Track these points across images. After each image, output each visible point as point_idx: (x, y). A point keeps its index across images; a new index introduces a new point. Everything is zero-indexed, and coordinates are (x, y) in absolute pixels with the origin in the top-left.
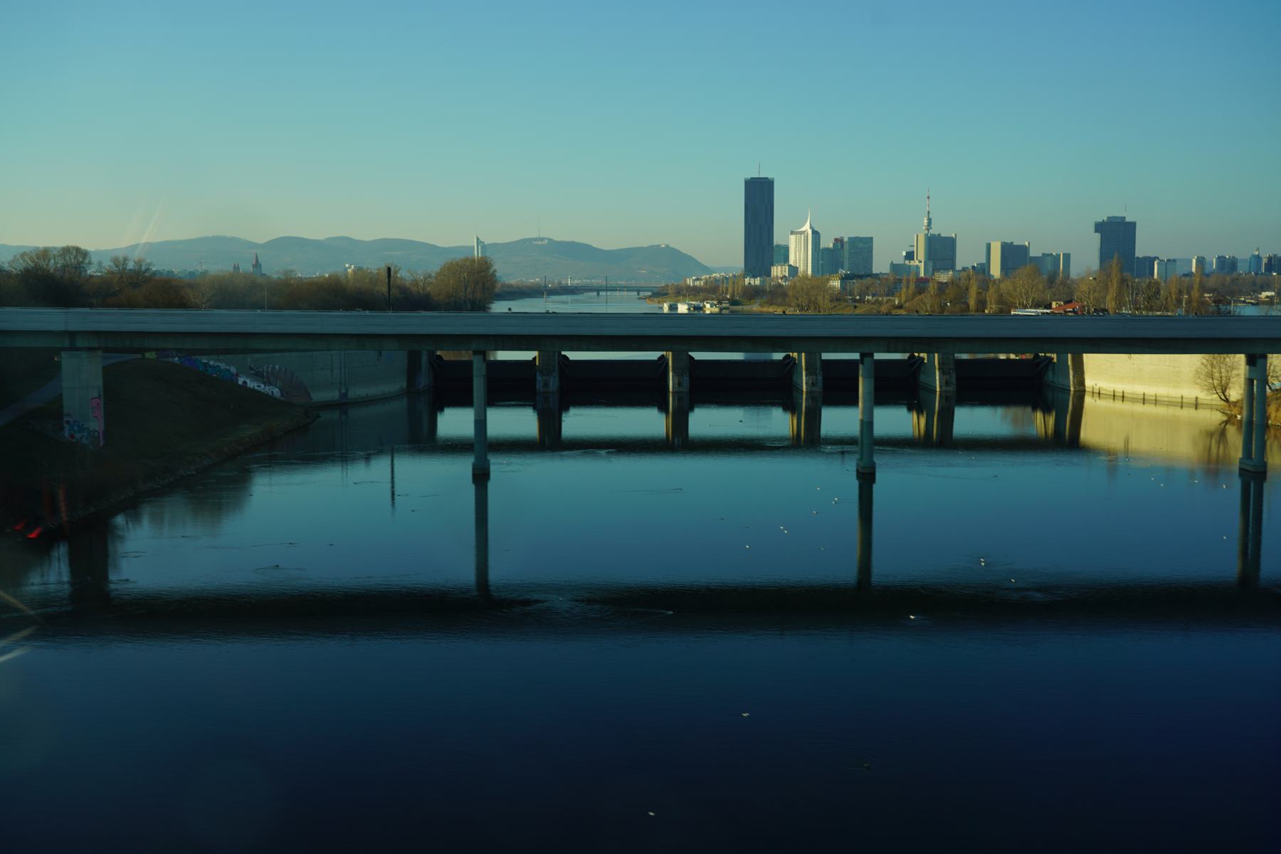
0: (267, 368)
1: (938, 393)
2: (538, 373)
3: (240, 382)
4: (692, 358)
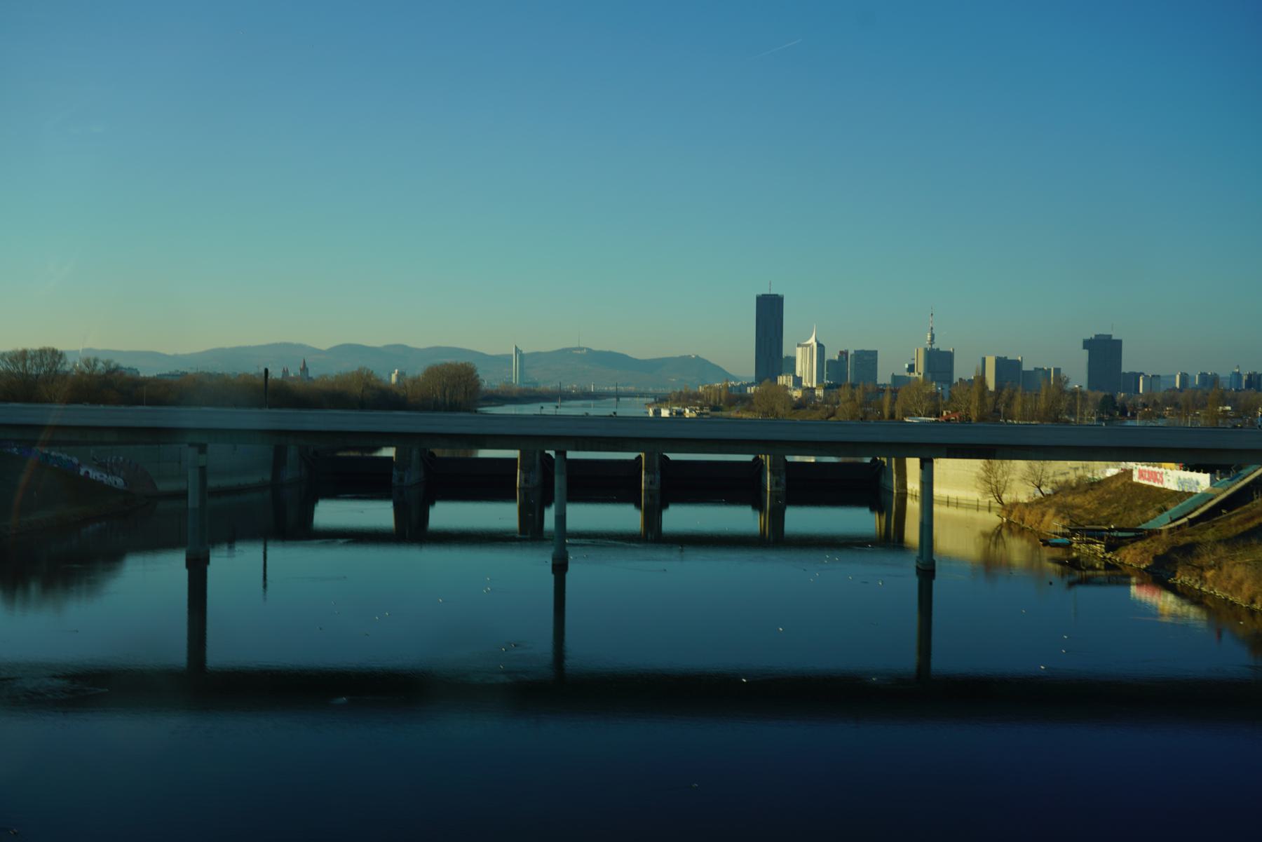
0: (111, 459)
1: (768, 493)
2: (394, 469)
3: (82, 472)
4: (667, 458)
